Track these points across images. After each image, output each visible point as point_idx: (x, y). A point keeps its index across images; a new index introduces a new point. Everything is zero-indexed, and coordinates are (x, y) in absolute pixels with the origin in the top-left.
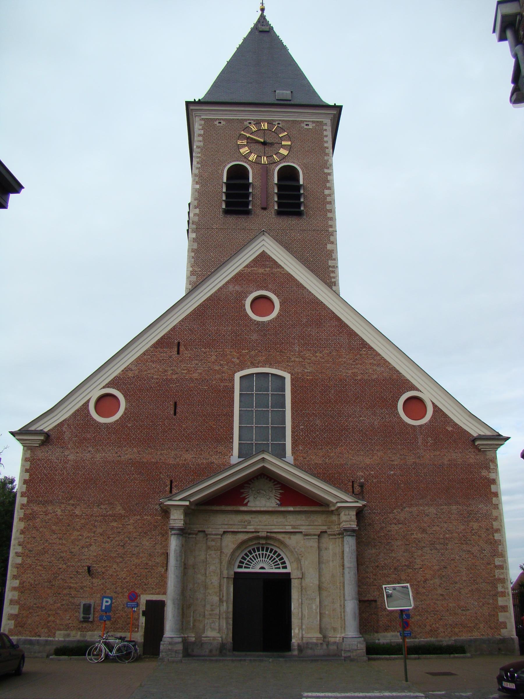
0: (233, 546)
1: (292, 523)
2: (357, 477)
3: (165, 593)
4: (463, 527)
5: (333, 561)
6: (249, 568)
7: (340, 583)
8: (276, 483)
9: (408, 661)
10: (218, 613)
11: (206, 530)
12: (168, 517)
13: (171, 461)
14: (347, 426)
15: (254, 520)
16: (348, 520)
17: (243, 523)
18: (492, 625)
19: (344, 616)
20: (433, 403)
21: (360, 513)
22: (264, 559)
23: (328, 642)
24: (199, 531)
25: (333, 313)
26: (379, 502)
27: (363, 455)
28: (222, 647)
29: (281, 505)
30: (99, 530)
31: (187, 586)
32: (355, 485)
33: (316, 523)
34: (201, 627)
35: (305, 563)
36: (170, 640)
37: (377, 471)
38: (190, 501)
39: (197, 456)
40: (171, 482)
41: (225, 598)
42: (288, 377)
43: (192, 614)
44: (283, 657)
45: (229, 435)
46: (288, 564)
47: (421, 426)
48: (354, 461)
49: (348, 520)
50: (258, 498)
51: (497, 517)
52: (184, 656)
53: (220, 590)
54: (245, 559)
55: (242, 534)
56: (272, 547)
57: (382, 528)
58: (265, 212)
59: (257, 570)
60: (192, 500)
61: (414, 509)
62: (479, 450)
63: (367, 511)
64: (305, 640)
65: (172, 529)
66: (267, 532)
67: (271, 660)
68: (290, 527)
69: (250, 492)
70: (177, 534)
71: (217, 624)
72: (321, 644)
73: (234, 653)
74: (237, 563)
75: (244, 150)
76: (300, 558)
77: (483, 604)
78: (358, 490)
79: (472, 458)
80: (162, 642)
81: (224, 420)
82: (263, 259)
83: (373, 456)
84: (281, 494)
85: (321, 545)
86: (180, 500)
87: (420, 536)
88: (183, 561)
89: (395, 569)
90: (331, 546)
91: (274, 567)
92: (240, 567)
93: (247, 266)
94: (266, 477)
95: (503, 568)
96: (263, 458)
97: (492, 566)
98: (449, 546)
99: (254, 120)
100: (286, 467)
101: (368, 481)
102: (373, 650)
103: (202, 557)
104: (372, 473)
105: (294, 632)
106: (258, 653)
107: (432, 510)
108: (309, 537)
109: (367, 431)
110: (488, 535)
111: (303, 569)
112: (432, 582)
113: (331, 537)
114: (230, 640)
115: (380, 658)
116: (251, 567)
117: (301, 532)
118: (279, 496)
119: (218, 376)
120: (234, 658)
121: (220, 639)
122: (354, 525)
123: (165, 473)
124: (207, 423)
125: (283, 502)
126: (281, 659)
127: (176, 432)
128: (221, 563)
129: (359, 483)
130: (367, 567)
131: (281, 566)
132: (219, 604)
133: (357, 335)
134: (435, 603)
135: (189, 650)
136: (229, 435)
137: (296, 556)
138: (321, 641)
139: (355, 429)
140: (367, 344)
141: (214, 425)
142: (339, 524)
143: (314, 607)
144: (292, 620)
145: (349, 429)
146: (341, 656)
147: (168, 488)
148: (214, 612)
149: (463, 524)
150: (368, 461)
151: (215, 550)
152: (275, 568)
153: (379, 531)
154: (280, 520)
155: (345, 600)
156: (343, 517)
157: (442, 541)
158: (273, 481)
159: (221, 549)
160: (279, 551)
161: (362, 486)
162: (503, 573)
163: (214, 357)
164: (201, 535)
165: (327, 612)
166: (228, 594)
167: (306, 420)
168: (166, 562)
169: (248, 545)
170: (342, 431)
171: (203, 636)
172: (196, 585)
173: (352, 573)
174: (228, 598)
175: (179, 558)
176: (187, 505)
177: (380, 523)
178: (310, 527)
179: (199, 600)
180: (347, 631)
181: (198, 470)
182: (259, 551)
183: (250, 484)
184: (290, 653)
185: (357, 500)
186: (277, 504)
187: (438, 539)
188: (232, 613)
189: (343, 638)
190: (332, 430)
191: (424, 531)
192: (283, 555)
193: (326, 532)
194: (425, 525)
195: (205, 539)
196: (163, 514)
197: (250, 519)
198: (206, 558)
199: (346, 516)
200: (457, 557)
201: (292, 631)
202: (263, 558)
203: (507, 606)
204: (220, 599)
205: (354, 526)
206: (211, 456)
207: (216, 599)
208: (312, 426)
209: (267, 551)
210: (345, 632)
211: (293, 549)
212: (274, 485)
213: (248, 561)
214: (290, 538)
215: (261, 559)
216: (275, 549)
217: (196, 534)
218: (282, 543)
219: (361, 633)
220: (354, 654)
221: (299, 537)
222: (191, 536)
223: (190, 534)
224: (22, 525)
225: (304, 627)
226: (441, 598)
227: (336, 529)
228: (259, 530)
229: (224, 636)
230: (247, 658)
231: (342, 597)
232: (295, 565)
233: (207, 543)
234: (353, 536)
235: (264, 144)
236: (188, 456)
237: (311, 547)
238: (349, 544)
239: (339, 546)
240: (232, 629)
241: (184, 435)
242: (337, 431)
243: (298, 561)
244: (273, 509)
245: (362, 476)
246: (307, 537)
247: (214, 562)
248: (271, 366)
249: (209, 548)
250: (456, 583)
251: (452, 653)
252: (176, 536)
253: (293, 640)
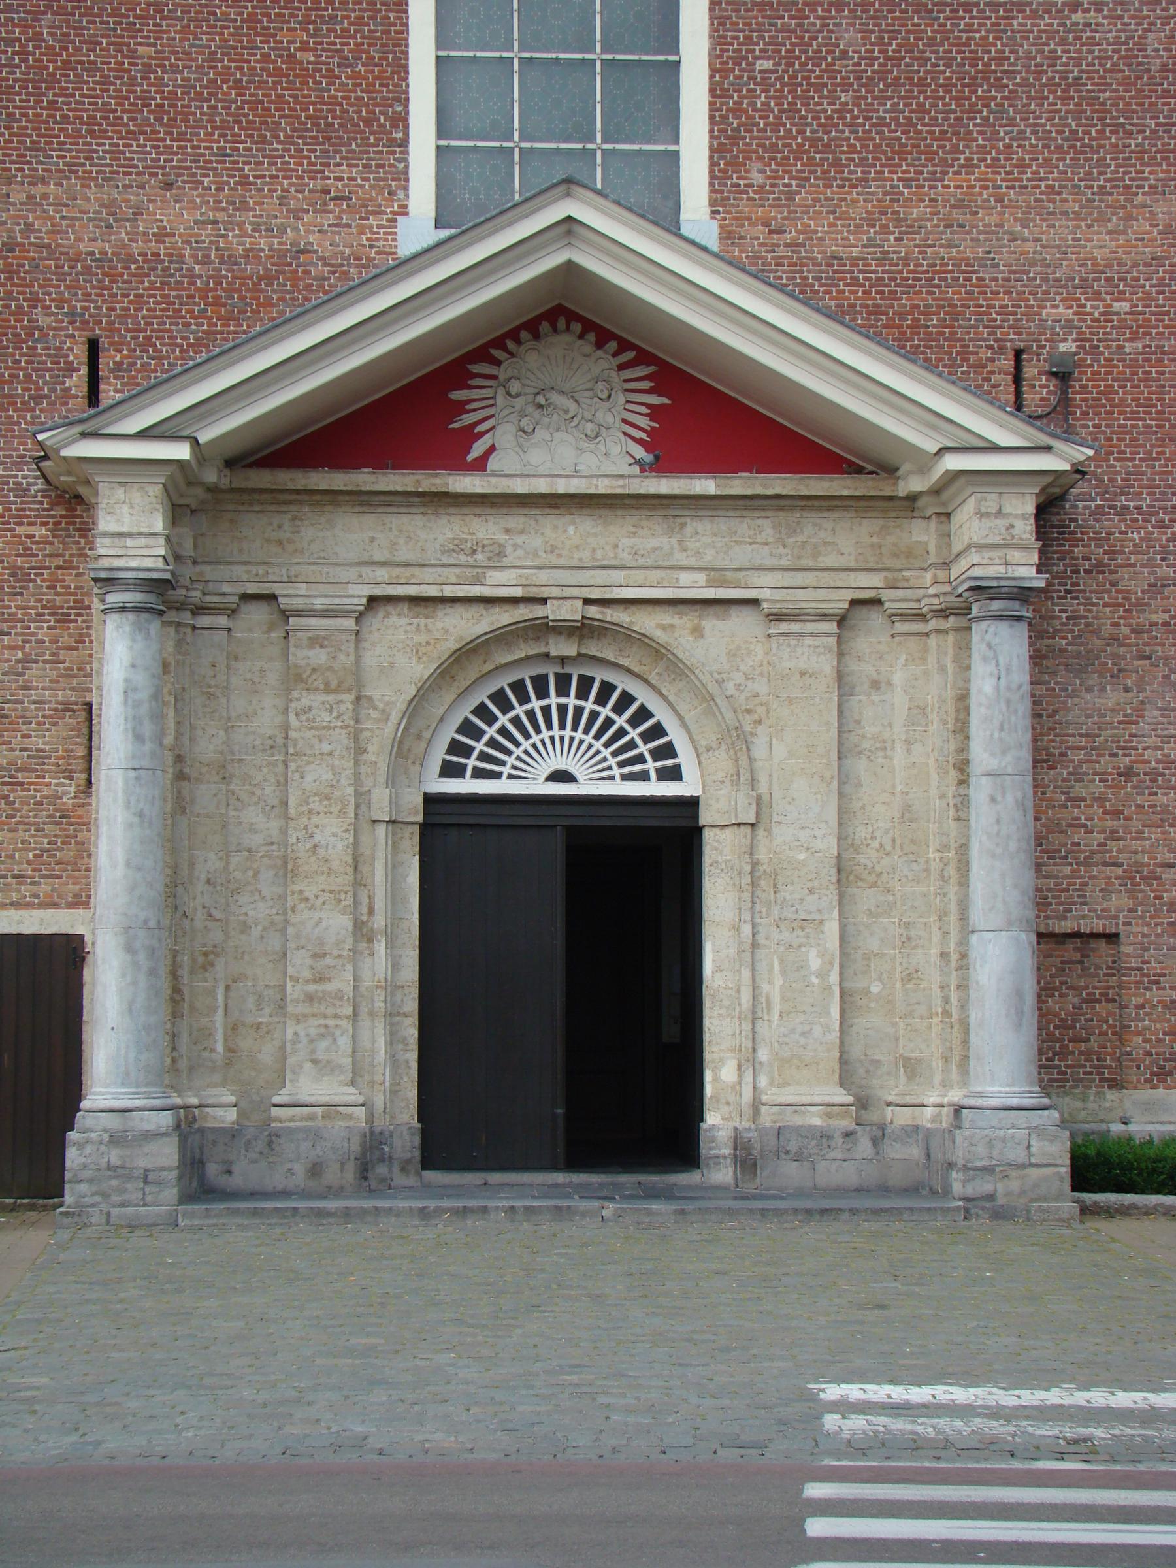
1: (709, 557)
2: (1042, 330)
3: (82, 901)
5: (908, 743)
6: (498, 775)
7: (944, 848)
8: (630, 355)
10: (348, 990)
11: (277, 589)
12: (86, 530)
13: (87, 240)
14: (1001, 58)
15: (519, 540)
16: (996, 540)
17: (463, 559)
19: (963, 1006)
21: (1052, 506)
22: (568, 733)
23: (882, 1128)
24: (246, 597)
26: (1148, 457)
27: (1078, 217)
28: (370, 1156)
29: (661, 464)
31: (192, 865)
33: (829, 561)
34: (267, 1054)
35: (773, 752)
36: (113, 1122)
37: (1147, 297)
38: (195, 442)
39: (221, 216)
40: (94, 348)
41: (379, 921)
43: (220, 997)
44: (667, 1194)
45: (386, 103)
46: (685, 757)
48: (1030, 246)
49: (997, 540)
50: (541, 434)
52: (187, 1198)
53: (357, 883)
54: (477, 734)
55: (460, 609)
56: (611, 677)
60: (204, 437)
63: (1082, 503)
64: (767, 1117)
65: (109, 582)
66: (587, 602)
67: (609, 1209)
68: (701, 578)
69: (500, 400)
70: (137, 609)
71: (344, 1042)
72: (848, 1134)
73: (429, 1175)
74: (439, 754)
76: (748, 728)
78: (1051, 393)
80: (72, 1136)
81: (360, 21)
83: (1129, 218)
84: (655, 412)
85: (852, 665)
86: (144, 435)
88: (169, 740)
90: (903, 675)
91: (617, 771)
92: (450, 770)
94: (577, 327)
96: (569, 219)
100: (684, 270)
101: (1095, 352)
102: (1101, 1170)
103: (266, 722)
104: (1125, 306)
105: (716, 1079)
108: (795, 627)
109: (1103, 86)
111: (763, 779)
113: (901, 627)
114: (408, 1114)
115: (1134, 1206)
116: (506, 770)
117: (755, 602)
118: (644, 422)
120: (431, 1204)
121: (360, 1112)
122: (1024, 568)
123: (60, 302)
124: (267, 35)
125: (669, 448)
126: (656, 1206)
127: (105, 81)
128: (360, 751)
129: (1050, 359)
130: (1078, 776)
131: (651, 765)
132: (353, 950)
135: (206, 1172)
136: (386, 103)
137: (729, 716)
138: (847, 1124)
139: (1039, 73)
141: (304, 47)
142: (946, 565)
143: (815, 963)
144: (707, 1022)
145: (1011, 74)
146: (947, 1192)
147: (77, 382)
148: (329, 987)
150: (1101, 246)
151: (328, 690)
152: (625, 777)
153: (1140, 603)
154: (654, 542)
155: (966, 930)
156: (970, 523)
158: (613, 345)
159: (359, 684)
160: (643, 696)
164: (257, 614)
165: (875, 988)
166: (395, 896)
167: (786, 29)
168: (81, 752)
169: (489, 667)
170: (973, 85)
171: (276, 1099)
172: (235, 860)
173: (1010, 798)
174: (395, 920)
175: (148, 729)
176: (179, 463)
177: (1150, 564)
178: (800, 578)
179: (256, 932)
180: (980, 1079)
181: (230, 291)
182: (542, 693)
183: (498, 363)
185: (1045, 440)
186: (638, 462)
188: (414, 993)
189: (958, 1110)
190: (922, 83)
192: (661, 714)
193: (876, 602)
195: (277, 634)
196: (60, 511)
197: (502, 537)
198: (286, 728)
199: (987, 523)
201: (708, 1076)
202: (562, 726)
204: (358, 925)
205: (1023, 572)
206: (297, 214)
207: (338, 923)
208: (818, 58)
209: (583, 694)
210: (964, 1083)
211: (712, 687)
212: (621, 367)
213: (492, 743)
214: (697, 632)
215: (556, 732)
216: (623, 684)
217: (233, 612)
218: (658, 652)
219: (1046, 1090)
220: (1015, 1185)
221: (742, 624)
222: (205, 620)
223: (199, 610)
225: (763, 1055)
227: (927, 589)
228: (545, 593)
229: (379, 1101)
230: (491, 1204)
231: (953, 918)
232: (721, 762)
233: (285, 654)
234: (1019, 618)
236: (178, 217)
237: (803, 674)
238: (999, 657)
239: (942, 669)
240: (415, 1066)
241: (146, 99)
242: (947, 87)
243: (738, 740)
244: (618, 487)
245: (1069, 326)
246: (784, 627)
247: (326, 747)
249: (295, 678)
252: (131, 616)
253: (712, 1118)
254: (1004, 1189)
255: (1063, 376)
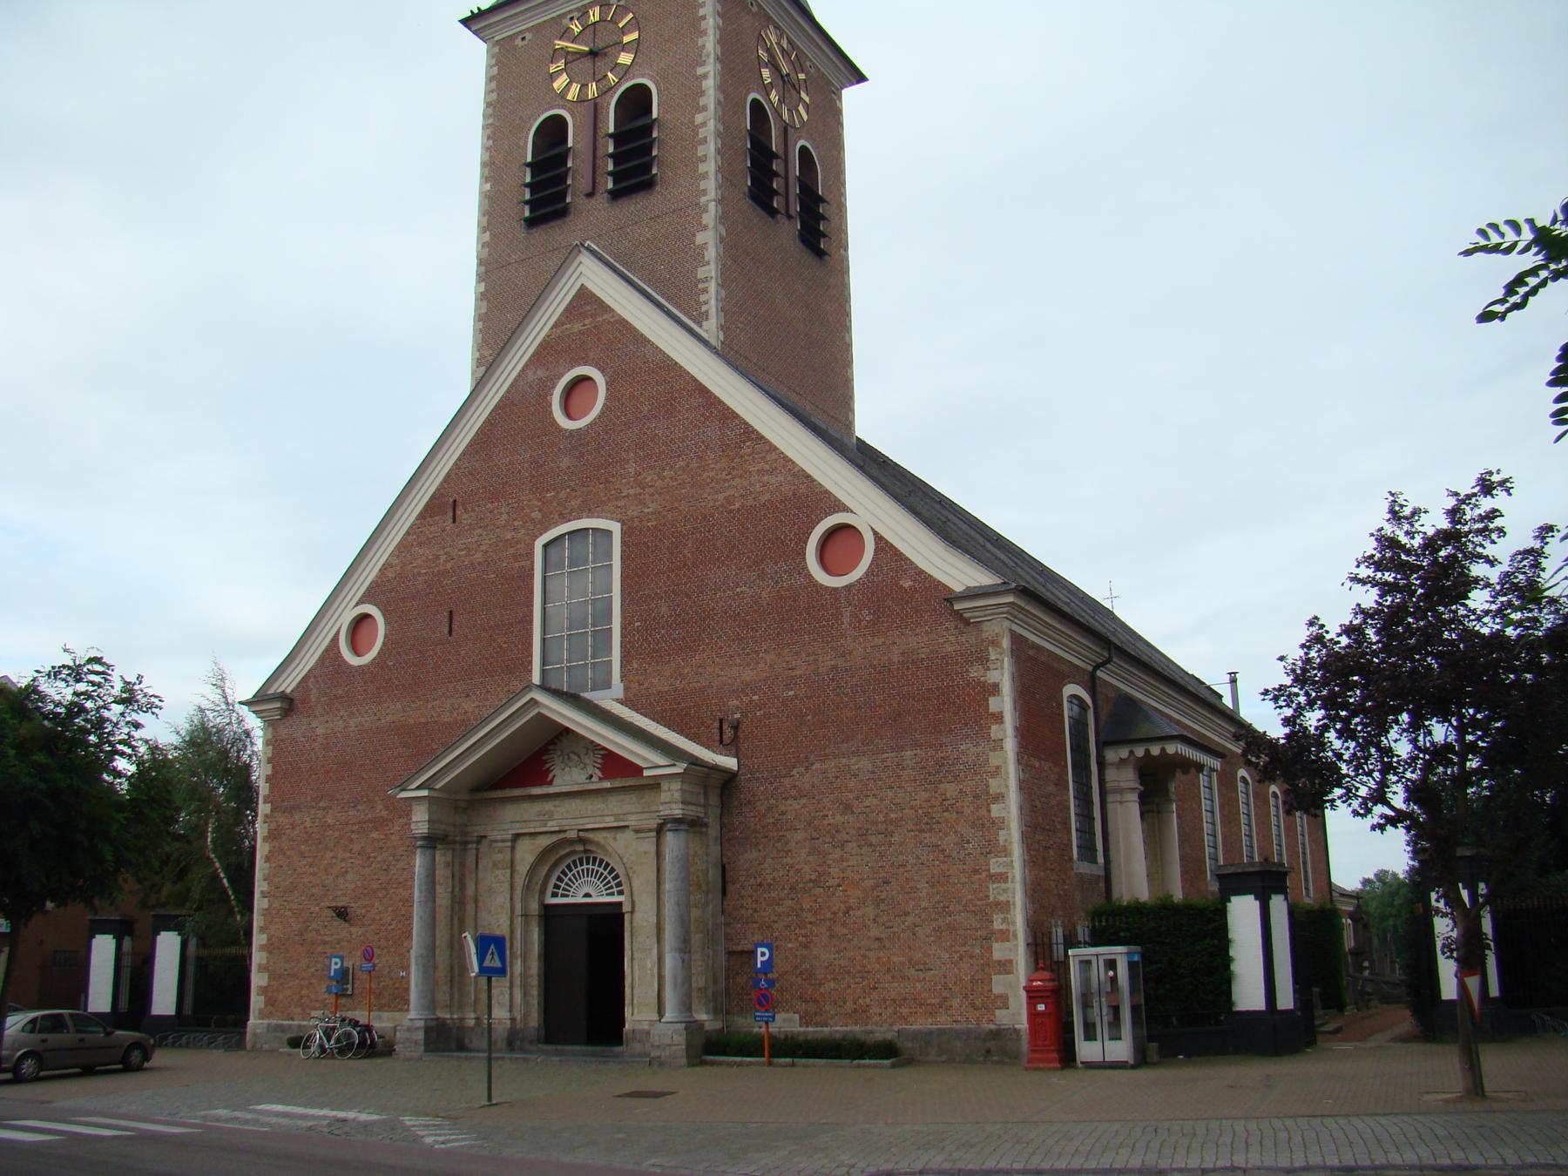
0: (530, 859)
1: (616, 811)
4: (925, 795)
9: (495, 1065)
13: (446, 718)
18: (978, 1003)
20: (875, 533)
25: (696, 380)
30: (356, 847)
32: (725, 727)
42: (615, 527)
47: (848, 588)
51: (998, 767)
57: (770, 809)
58: (593, 201)
59: (580, 900)
61: (830, 765)
62: (967, 622)
74: (550, 889)
75: (560, 83)
77: (961, 958)
79: (950, 641)
82: (585, 300)
86: (419, 788)
87: (839, 819)
89: (792, 888)
92: (555, 895)
93: (555, 326)
95: (1006, 881)
97: (984, 875)
98: (896, 838)
99: (577, 9)
106: (578, 1048)
107: (865, 764)
110: (978, 808)
112: (859, 913)
114: (535, 1019)
119: (511, 551)
130: (743, 887)
133: (737, 416)
134: (864, 957)
135: (443, 1038)
140: (754, 431)
149: (926, 790)
150: (748, 675)
157: (882, 827)
161: (736, 727)
162: (1005, 891)
163: (505, 516)
184: (619, 1049)
187: (875, 823)
191: (847, 808)
194: (851, 796)
200: (912, 861)
203: (1010, 961)
221: (629, 835)
224: (994, 704)
226: (877, 944)
235: (593, 54)
248: (591, 514)
250: (906, 914)
251: (861, 1057)
253: (7, 1032)
254: (664, 1054)
255: (736, 728)
